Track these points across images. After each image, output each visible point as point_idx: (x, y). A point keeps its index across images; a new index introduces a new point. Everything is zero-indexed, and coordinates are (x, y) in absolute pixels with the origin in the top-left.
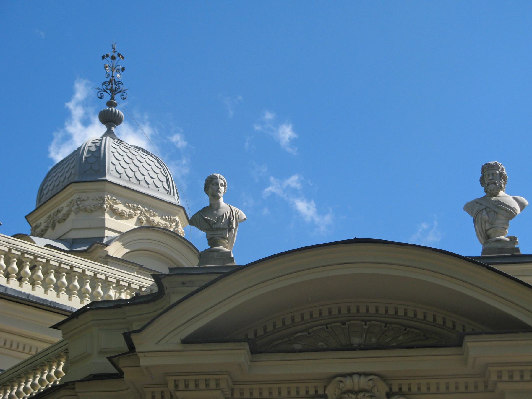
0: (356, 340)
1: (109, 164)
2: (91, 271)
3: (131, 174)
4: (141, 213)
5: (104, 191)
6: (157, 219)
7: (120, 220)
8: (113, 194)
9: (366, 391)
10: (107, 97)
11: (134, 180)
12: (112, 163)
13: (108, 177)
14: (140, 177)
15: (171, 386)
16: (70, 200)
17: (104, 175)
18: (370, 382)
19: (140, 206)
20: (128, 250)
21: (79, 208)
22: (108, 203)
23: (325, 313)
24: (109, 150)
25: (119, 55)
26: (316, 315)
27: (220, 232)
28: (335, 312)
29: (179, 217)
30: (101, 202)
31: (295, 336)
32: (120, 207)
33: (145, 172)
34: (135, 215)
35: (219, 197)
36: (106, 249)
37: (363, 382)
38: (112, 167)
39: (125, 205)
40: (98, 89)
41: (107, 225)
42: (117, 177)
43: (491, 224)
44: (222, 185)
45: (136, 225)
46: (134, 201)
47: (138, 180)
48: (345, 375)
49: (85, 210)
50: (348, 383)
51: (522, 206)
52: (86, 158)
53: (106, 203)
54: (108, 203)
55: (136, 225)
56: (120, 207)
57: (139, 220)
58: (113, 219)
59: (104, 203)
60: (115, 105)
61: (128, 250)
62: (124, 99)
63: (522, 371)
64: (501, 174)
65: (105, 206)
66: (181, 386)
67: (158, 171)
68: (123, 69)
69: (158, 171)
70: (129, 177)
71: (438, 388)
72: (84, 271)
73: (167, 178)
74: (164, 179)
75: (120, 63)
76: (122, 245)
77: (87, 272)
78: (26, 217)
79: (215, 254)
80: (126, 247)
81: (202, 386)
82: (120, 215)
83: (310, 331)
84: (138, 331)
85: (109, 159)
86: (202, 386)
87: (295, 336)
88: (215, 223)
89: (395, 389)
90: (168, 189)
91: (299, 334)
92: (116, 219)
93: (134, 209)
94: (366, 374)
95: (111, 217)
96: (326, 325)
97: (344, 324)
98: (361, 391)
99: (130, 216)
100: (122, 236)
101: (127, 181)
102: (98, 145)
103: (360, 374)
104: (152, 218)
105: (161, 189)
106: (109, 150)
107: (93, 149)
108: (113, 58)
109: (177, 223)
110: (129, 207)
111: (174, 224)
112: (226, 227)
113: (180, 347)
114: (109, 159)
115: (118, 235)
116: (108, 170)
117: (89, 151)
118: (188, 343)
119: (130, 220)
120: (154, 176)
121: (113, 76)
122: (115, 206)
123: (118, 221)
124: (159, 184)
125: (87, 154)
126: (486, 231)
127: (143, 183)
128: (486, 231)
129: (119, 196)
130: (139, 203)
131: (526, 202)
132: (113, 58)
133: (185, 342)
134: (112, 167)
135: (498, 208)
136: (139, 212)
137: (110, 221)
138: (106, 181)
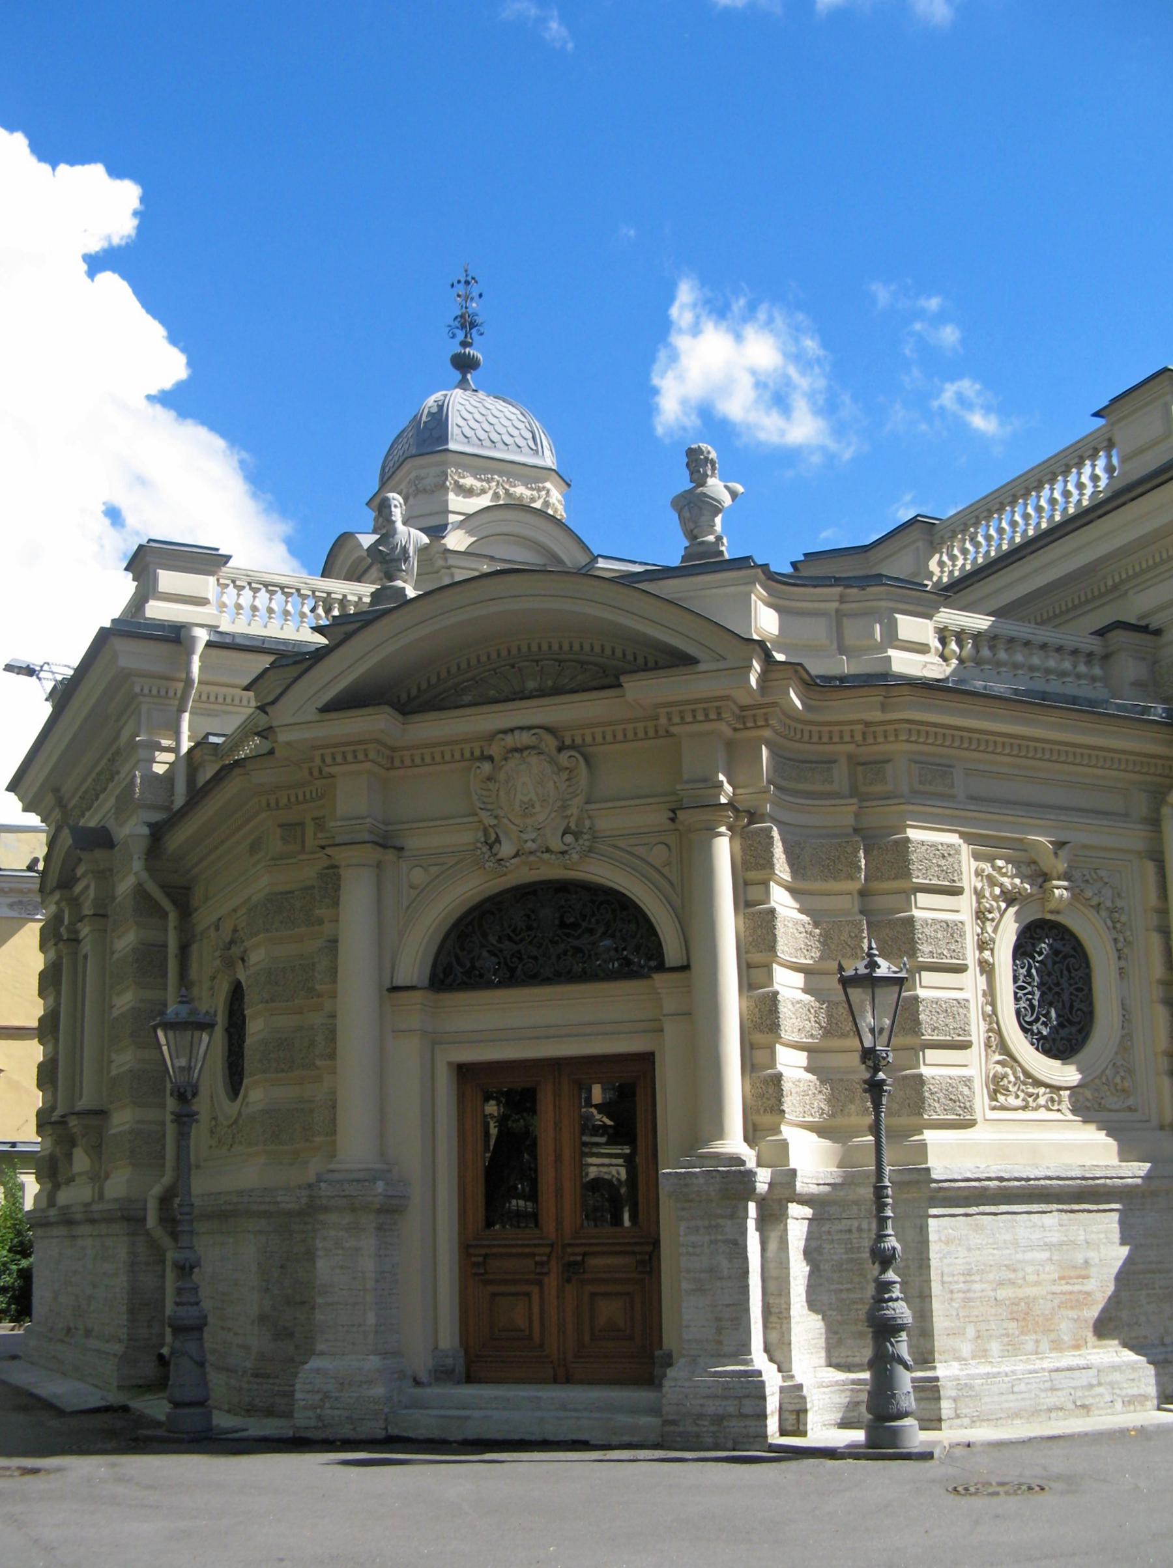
0: (531, 685)
1: (452, 428)
2: (355, 594)
3: (482, 435)
4: (498, 485)
5: (446, 464)
6: (520, 490)
7: (469, 497)
8: (458, 465)
9: (533, 748)
10: (460, 335)
11: (488, 443)
12: (457, 425)
13: (452, 446)
14: (495, 437)
15: (318, 761)
16: (408, 479)
17: (447, 442)
18: (534, 737)
19: (496, 477)
20: (474, 539)
21: (417, 489)
22: (453, 479)
23: (494, 656)
24: (453, 408)
25: (473, 278)
26: (484, 659)
27: (394, 564)
28: (504, 653)
29: (552, 483)
30: (443, 478)
31: (462, 686)
32: (469, 481)
33: (502, 430)
34: (490, 489)
35: (394, 522)
36: (443, 542)
37: (525, 738)
38: (456, 428)
39: (476, 478)
40: (449, 326)
41: (451, 508)
42: (463, 443)
43: (695, 522)
44: (396, 506)
45: (491, 501)
46: (486, 471)
47: (493, 442)
48: (505, 732)
49: (425, 491)
50: (510, 740)
51: (734, 495)
52: (425, 422)
53: (450, 478)
54: (453, 479)
55: (491, 501)
56: (469, 481)
57: (496, 495)
58: (460, 498)
59: (446, 479)
60: (470, 345)
61: (474, 539)
62: (482, 334)
63: (694, 711)
64: (706, 459)
65: (448, 483)
66: (328, 760)
67: (520, 426)
68: (481, 295)
69: (520, 426)
70: (480, 440)
71: (636, 734)
72: (345, 596)
73: (533, 433)
74: (529, 436)
75: (475, 290)
76: (466, 533)
77: (350, 598)
78: (367, 504)
79: (388, 592)
80: (472, 536)
81: (350, 758)
82: (469, 492)
83: (477, 678)
84: (273, 703)
85: (452, 421)
86: (350, 758)
87: (462, 686)
88: (388, 554)
89: (568, 742)
90: (534, 447)
91: (465, 684)
92: (464, 497)
93: (488, 481)
94: (530, 728)
95: (457, 495)
96: (494, 670)
97: (513, 667)
98: (527, 748)
99: (483, 491)
100: (469, 520)
101: (478, 446)
102: (440, 403)
103: (521, 728)
104: (512, 490)
105: (526, 450)
106: (453, 408)
107: (434, 410)
108: (467, 283)
109: (548, 491)
110: (481, 480)
111: (544, 493)
112: (401, 556)
113: (318, 717)
114: (454, 420)
115: (462, 518)
116: (452, 435)
117: (429, 413)
118: (329, 711)
119: (483, 496)
120: (515, 432)
121: (466, 308)
122: (462, 481)
123: (467, 500)
124: (522, 443)
125: (427, 417)
126: (692, 531)
127: (500, 445)
128: (692, 531)
129: (466, 468)
130: (493, 472)
131: (740, 489)
132: (467, 283)
133: (327, 709)
134: (457, 431)
135: (704, 501)
136: (494, 484)
137: (455, 502)
138: (447, 450)
